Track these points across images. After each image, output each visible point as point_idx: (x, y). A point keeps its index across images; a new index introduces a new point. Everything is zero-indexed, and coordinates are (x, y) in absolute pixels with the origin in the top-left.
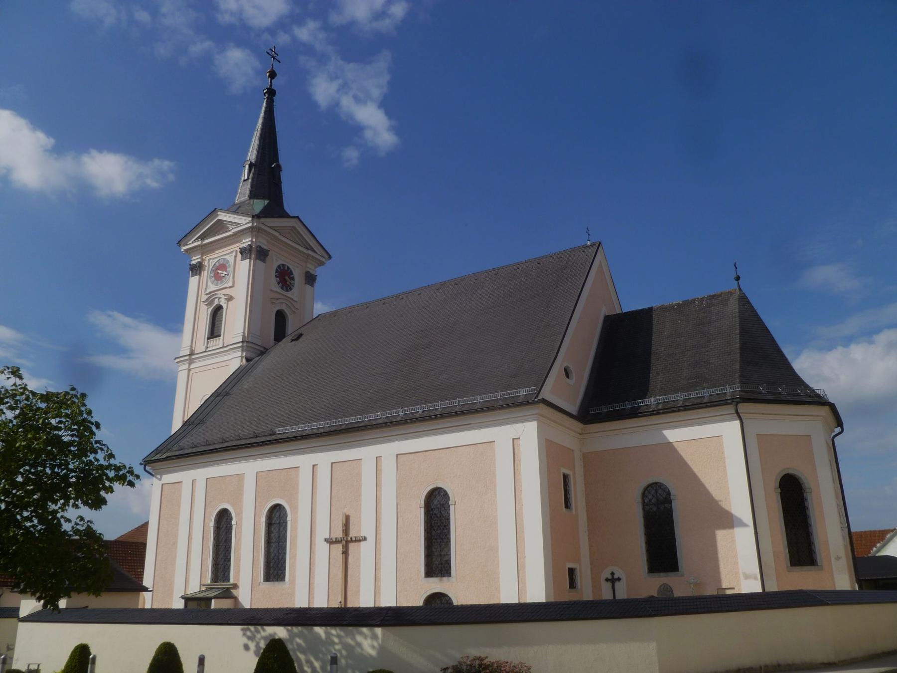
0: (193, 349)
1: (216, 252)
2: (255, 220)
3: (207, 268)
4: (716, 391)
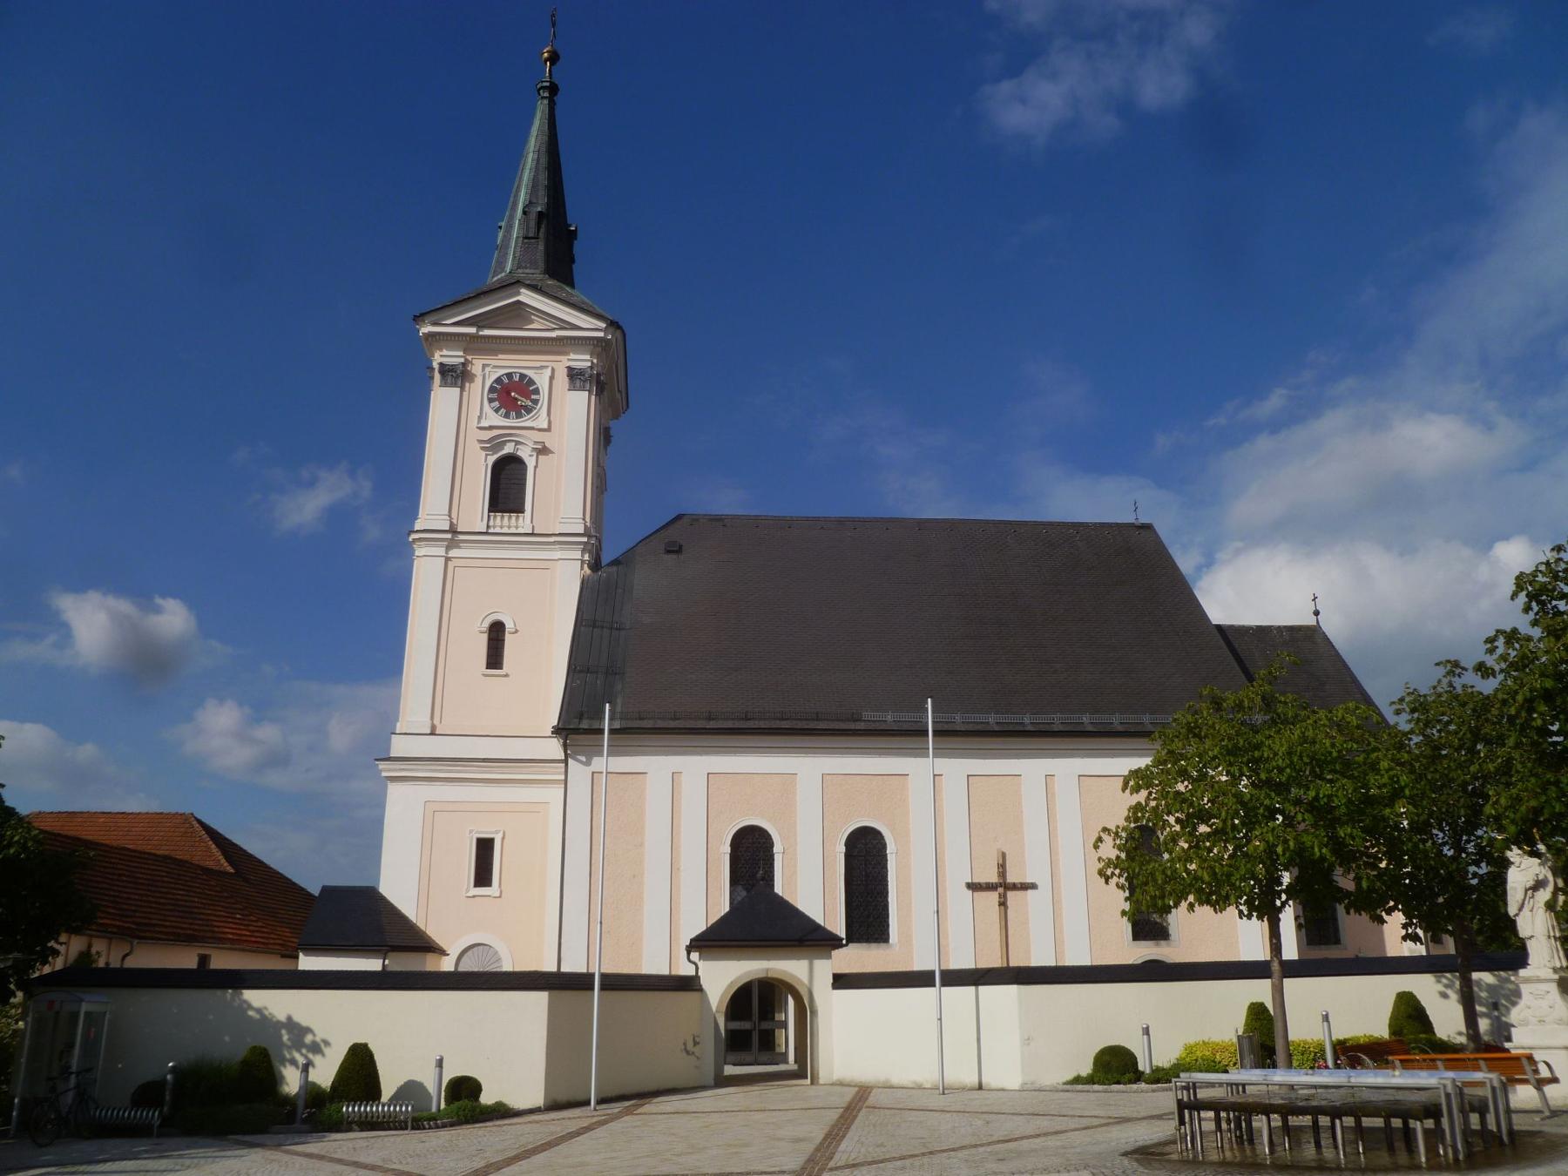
0: (455, 521)
1: (500, 356)
2: (611, 329)
3: (479, 380)
4: (1132, 718)
